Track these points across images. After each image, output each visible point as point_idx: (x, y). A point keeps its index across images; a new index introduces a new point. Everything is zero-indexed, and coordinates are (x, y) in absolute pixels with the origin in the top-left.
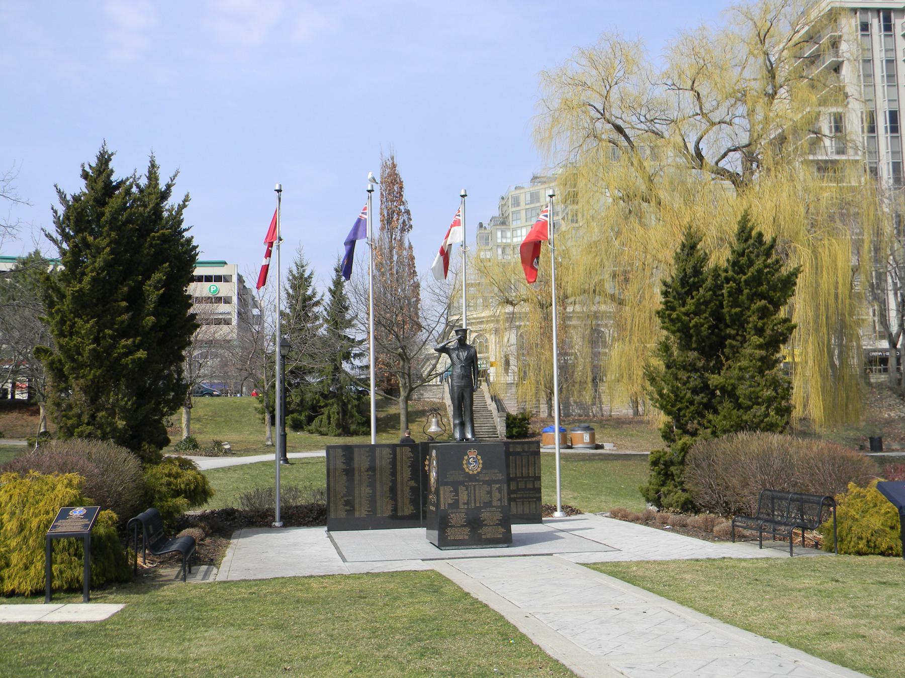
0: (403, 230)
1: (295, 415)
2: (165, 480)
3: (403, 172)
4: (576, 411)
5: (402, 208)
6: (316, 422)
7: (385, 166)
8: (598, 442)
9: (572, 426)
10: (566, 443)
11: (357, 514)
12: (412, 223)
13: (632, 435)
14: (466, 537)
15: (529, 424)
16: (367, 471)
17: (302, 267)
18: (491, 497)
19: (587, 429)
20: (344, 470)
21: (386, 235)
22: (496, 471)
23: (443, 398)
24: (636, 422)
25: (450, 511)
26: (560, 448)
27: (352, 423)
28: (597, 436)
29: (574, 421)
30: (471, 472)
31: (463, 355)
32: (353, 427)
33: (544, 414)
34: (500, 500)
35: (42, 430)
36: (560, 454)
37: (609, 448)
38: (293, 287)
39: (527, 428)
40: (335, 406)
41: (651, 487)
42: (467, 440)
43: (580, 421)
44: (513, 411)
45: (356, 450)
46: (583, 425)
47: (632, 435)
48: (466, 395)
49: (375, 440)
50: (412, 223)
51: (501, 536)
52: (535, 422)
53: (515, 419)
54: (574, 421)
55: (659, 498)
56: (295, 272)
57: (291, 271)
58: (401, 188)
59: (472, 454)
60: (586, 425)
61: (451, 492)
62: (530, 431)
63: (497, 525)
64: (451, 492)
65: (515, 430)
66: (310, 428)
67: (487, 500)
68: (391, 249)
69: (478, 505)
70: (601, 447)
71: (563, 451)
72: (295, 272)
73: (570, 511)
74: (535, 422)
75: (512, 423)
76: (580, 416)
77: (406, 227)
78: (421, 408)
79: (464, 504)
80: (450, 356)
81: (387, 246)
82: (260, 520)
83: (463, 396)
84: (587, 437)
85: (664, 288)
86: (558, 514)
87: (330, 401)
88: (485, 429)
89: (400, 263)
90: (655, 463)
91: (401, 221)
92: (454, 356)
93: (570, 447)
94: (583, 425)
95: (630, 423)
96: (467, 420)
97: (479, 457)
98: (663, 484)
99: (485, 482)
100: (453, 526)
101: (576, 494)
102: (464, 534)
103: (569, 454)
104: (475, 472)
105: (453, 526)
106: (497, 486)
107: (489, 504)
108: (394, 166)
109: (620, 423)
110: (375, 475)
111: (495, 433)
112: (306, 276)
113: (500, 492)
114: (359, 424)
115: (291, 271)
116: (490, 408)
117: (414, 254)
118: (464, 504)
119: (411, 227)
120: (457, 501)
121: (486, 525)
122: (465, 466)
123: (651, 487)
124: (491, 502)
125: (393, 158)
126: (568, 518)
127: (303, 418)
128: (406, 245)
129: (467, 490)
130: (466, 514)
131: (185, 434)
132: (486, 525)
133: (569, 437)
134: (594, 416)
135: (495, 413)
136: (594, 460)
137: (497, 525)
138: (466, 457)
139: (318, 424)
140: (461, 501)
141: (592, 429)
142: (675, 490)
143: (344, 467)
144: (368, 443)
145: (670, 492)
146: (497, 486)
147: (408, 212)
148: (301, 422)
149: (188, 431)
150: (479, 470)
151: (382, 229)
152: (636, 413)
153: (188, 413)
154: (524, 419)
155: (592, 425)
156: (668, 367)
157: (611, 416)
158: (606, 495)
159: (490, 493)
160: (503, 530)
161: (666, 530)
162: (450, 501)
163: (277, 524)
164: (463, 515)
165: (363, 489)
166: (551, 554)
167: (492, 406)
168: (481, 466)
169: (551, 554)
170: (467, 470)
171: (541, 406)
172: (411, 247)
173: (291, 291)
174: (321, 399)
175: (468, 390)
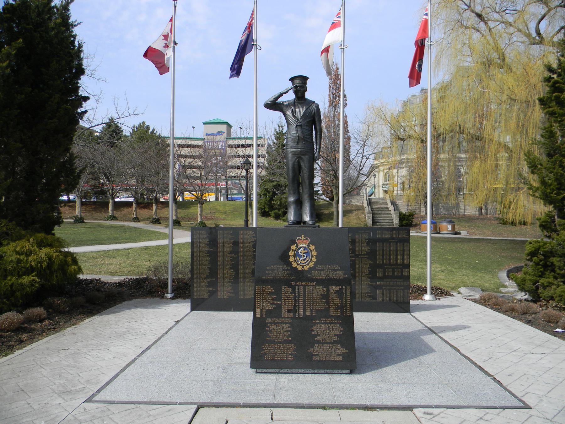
1: (276, 211)
2: (14, 257)
4: (443, 212)
8: (457, 231)
9: (439, 221)
10: (436, 229)
11: (219, 295)
13: (478, 227)
14: (291, 358)
15: (413, 218)
16: (231, 253)
17: (282, 127)
18: (328, 303)
19: (450, 222)
20: (208, 252)
21: (332, 110)
22: (336, 267)
23: (363, 203)
24: (481, 219)
25: (269, 320)
26: (431, 233)
28: (456, 227)
29: (441, 218)
30: (300, 268)
31: (300, 111)
33: (423, 214)
34: (340, 307)
35: (134, 216)
37: (464, 234)
38: (277, 138)
39: (412, 221)
41: (528, 277)
42: (305, 223)
43: (446, 218)
44: (404, 210)
45: (219, 232)
46: (447, 220)
47: (478, 227)
48: (304, 165)
50: (347, 102)
51: (340, 358)
52: (417, 218)
53: (404, 215)
54: (441, 218)
55: (537, 289)
56: (278, 130)
57: (276, 130)
59: (303, 243)
60: (450, 220)
61: (271, 293)
62: (414, 223)
63: (335, 342)
64: (271, 293)
65: (404, 222)
66: (284, 218)
67: (321, 305)
68: (334, 117)
69: (308, 313)
70: (459, 233)
71: (433, 235)
73: (439, 292)
74: (417, 218)
75: (403, 218)
76: (445, 214)
78: (350, 208)
79: (289, 311)
80: (285, 114)
81: (332, 116)
82: (160, 289)
83: (300, 167)
84: (450, 227)
85: (547, 74)
86: (427, 297)
88: (387, 221)
90: (533, 254)
92: (289, 113)
93: (439, 233)
94: (447, 220)
95: (477, 219)
96: (306, 197)
97: (312, 247)
98: (542, 276)
99: (320, 282)
100: (272, 342)
101: (443, 268)
102: (288, 353)
103: (438, 237)
105: (272, 342)
106: (337, 288)
107: (325, 313)
109: (470, 219)
110: (238, 257)
111: (392, 223)
112: (284, 132)
113: (341, 297)
115: (276, 130)
116: (390, 209)
117: (348, 120)
118: (289, 311)
120: (279, 307)
121: (319, 342)
122: (292, 259)
123: (528, 277)
124: (327, 310)
126: (438, 302)
127: (280, 213)
129: (294, 291)
130: (292, 325)
131: (199, 220)
132: (319, 342)
133: (438, 227)
134: (454, 215)
135: (393, 211)
136: (455, 242)
137: (335, 342)
138: (294, 247)
140: (285, 308)
141: (453, 222)
142: (556, 282)
143: (207, 248)
145: (550, 284)
146: (337, 288)
148: (280, 215)
149: (201, 218)
150: (311, 265)
151: (330, 106)
153: (201, 207)
154: (410, 215)
155: (453, 220)
156: (549, 155)
157: (464, 215)
158: (465, 269)
159: (326, 297)
160: (344, 350)
161: (555, 334)
162: (270, 307)
163: (169, 296)
164: (287, 327)
165: (226, 270)
166: (409, 408)
167: (391, 208)
168: (314, 259)
169: (409, 408)
170: (294, 265)
173: (275, 141)
175: (306, 158)
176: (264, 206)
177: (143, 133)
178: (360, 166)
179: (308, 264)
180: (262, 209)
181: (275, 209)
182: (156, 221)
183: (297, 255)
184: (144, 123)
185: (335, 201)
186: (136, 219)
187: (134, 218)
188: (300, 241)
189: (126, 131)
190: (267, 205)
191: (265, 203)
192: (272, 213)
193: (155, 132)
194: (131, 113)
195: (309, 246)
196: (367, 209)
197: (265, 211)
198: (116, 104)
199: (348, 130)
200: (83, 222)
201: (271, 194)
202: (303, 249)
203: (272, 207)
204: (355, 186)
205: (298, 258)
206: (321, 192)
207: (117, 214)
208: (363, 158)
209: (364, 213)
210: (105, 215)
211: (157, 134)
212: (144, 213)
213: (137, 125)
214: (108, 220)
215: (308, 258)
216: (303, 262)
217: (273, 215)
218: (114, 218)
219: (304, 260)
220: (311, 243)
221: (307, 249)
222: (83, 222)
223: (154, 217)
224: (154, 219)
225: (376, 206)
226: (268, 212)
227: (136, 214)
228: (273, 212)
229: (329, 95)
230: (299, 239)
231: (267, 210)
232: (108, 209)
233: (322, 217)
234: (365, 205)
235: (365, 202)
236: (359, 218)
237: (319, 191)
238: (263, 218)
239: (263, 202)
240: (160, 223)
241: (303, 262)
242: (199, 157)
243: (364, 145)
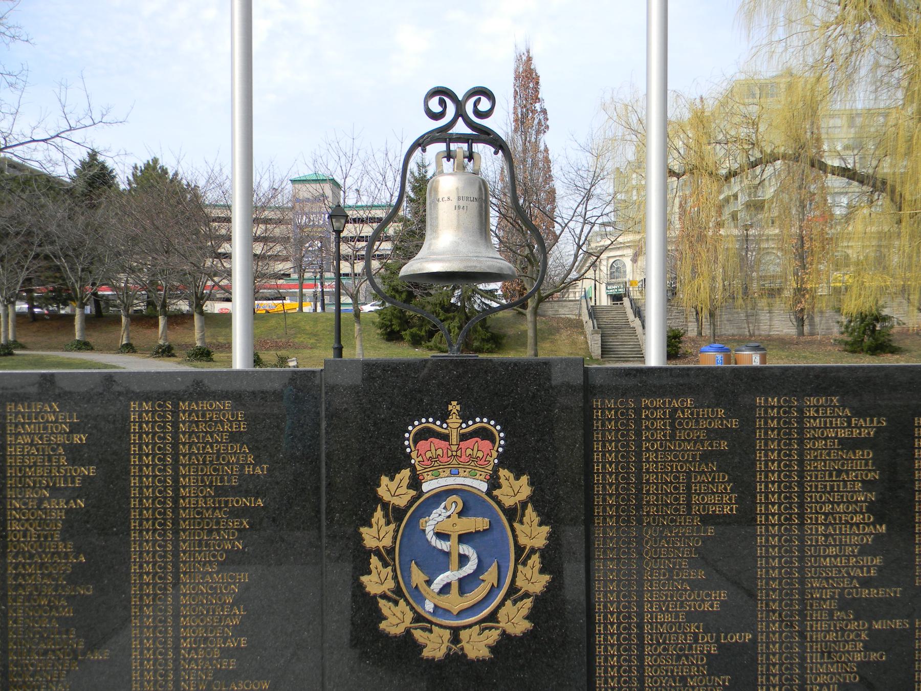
0: (538, 132)
1: (414, 330)
3: (539, 66)
5: (538, 106)
6: (436, 338)
7: (519, 59)
12: (548, 123)
15: (680, 342)
17: (424, 166)
19: (757, 348)
23: (580, 315)
27: (476, 339)
32: (476, 344)
35: (124, 342)
36: (255, 318)
40: (457, 320)
49: (202, 338)
50: (548, 123)
56: (416, 174)
58: (537, 83)
60: (757, 344)
62: (681, 351)
72: (416, 174)
77: (542, 128)
87: (451, 314)
89: (534, 164)
91: (536, 122)
97: (516, 489)
104: (516, 620)
108: (529, 59)
112: (428, 177)
114: (483, 340)
119: (547, 127)
125: (528, 52)
127: (423, 333)
128: (542, 148)
139: (438, 340)
144: (188, 340)
147: (544, 112)
148: (421, 338)
151: (516, 130)
152: (801, 333)
171: (690, 324)
172: (546, 150)
174: (441, 312)
176: (391, 321)
177: (152, 177)
178: (580, 239)
179: (493, 617)
180: (387, 326)
181: (411, 328)
182: (163, 352)
183: (413, 552)
184: (155, 161)
185: (529, 309)
186: (129, 348)
187: (123, 346)
188: (433, 447)
189: (123, 177)
190: (398, 318)
191: (393, 314)
192: (406, 334)
193: (179, 177)
194: (97, 119)
195: (494, 483)
196: (589, 325)
197: (392, 332)
198: (63, 100)
199: (550, 176)
200: (11, 354)
201: (404, 296)
202: (453, 504)
203: (407, 322)
204: (568, 280)
205: (418, 576)
206: (500, 292)
207: (94, 338)
208: (584, 223)
209: (583, 333)
210: (64, 339)
211: (184, 182)
212: (142, 336)
213: (141, 165)
214: (71, 350)
215: (490, 576)
216: (455, 602)
217: (408, 338)
218: (84, 346)
219: (465, 585)
220: (512, 460)
221: (484, 511)
222: (11, 354)
223: (161, 342)
224: (160, 347)
225: (606, 319)
226: (399, 332)
227: (128, 337)
228: (408, 332)
229: (515, 108)
230: (424, 435)
231: (396, 328)
232: (74, 326)
233: (504, 341)
234: (585, 317)
235: (585, 312)
236: (574, 343)
237: (497, 290)
238: (389, 344)
239: (389, 313)
240: (173, 355)
241: (455, 602)
242: (285, 240)
243: (588, 196)
